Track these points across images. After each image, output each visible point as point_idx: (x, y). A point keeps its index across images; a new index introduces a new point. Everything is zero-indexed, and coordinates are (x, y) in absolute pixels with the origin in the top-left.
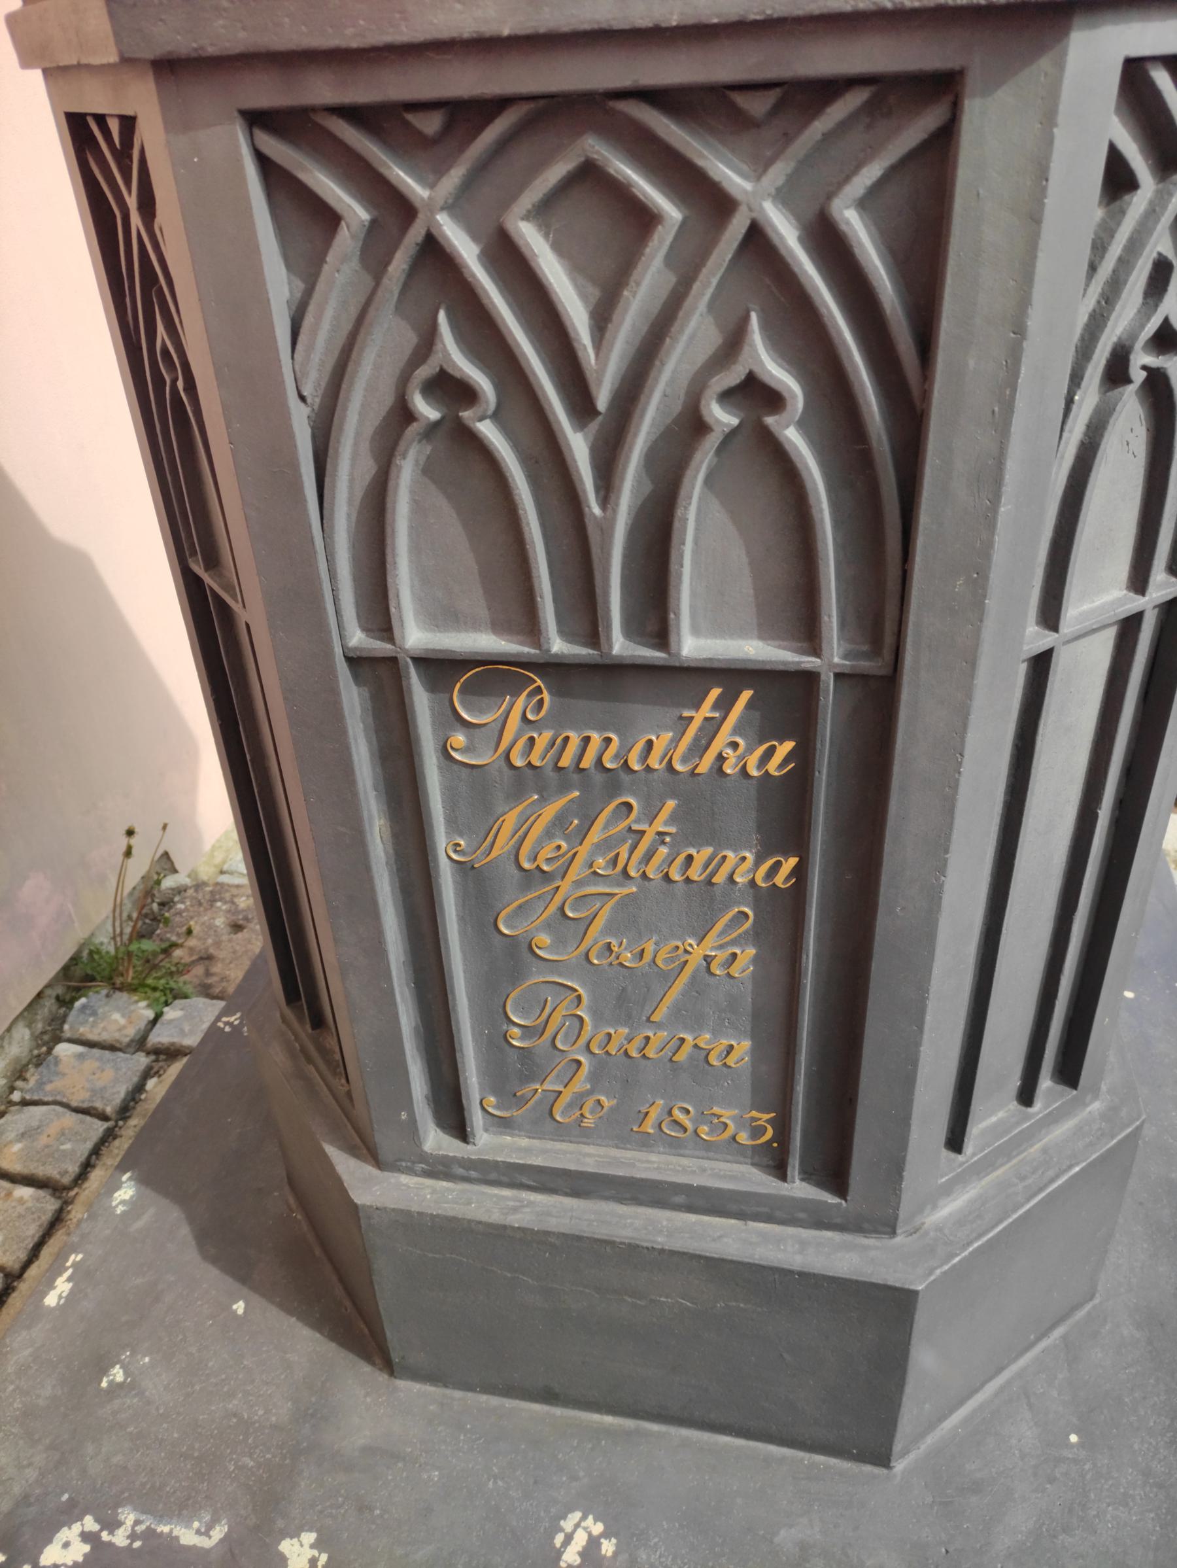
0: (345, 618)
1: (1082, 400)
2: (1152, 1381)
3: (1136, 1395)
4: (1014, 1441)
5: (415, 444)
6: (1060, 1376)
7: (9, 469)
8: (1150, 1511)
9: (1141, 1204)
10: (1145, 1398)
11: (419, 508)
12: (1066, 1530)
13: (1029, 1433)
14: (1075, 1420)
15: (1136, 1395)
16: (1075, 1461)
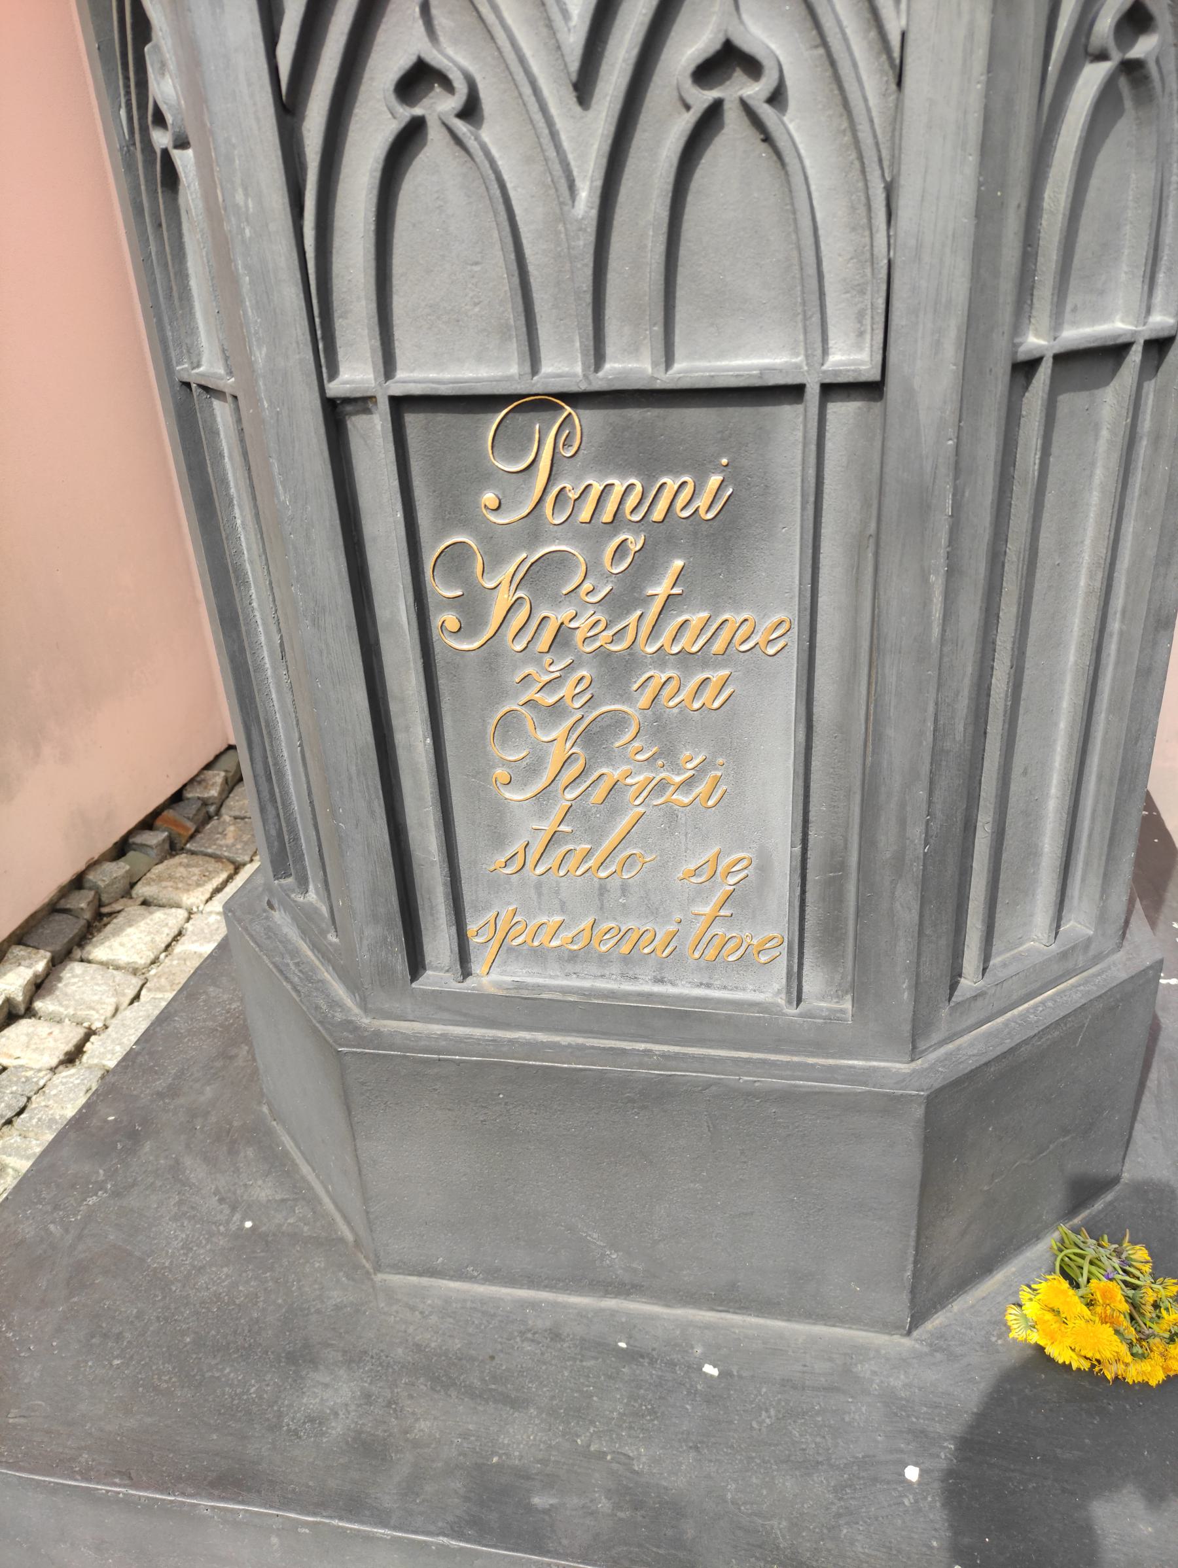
0: (820, 585)
1: (196, 90)
2: (280, 1301)
3: (270, 1284)
4: (260, 1182)
5: (786, 119)
6: (306, 1228)
7: (391, 7)
8: (171, 1263)
9: (492, 1358)
10: (266, 1289)
11: (163, 197)
12: (180, 1203)
13: (263, 1194)
14: (264, 1229)
15: (270, 1284)
16: (228, 1222)
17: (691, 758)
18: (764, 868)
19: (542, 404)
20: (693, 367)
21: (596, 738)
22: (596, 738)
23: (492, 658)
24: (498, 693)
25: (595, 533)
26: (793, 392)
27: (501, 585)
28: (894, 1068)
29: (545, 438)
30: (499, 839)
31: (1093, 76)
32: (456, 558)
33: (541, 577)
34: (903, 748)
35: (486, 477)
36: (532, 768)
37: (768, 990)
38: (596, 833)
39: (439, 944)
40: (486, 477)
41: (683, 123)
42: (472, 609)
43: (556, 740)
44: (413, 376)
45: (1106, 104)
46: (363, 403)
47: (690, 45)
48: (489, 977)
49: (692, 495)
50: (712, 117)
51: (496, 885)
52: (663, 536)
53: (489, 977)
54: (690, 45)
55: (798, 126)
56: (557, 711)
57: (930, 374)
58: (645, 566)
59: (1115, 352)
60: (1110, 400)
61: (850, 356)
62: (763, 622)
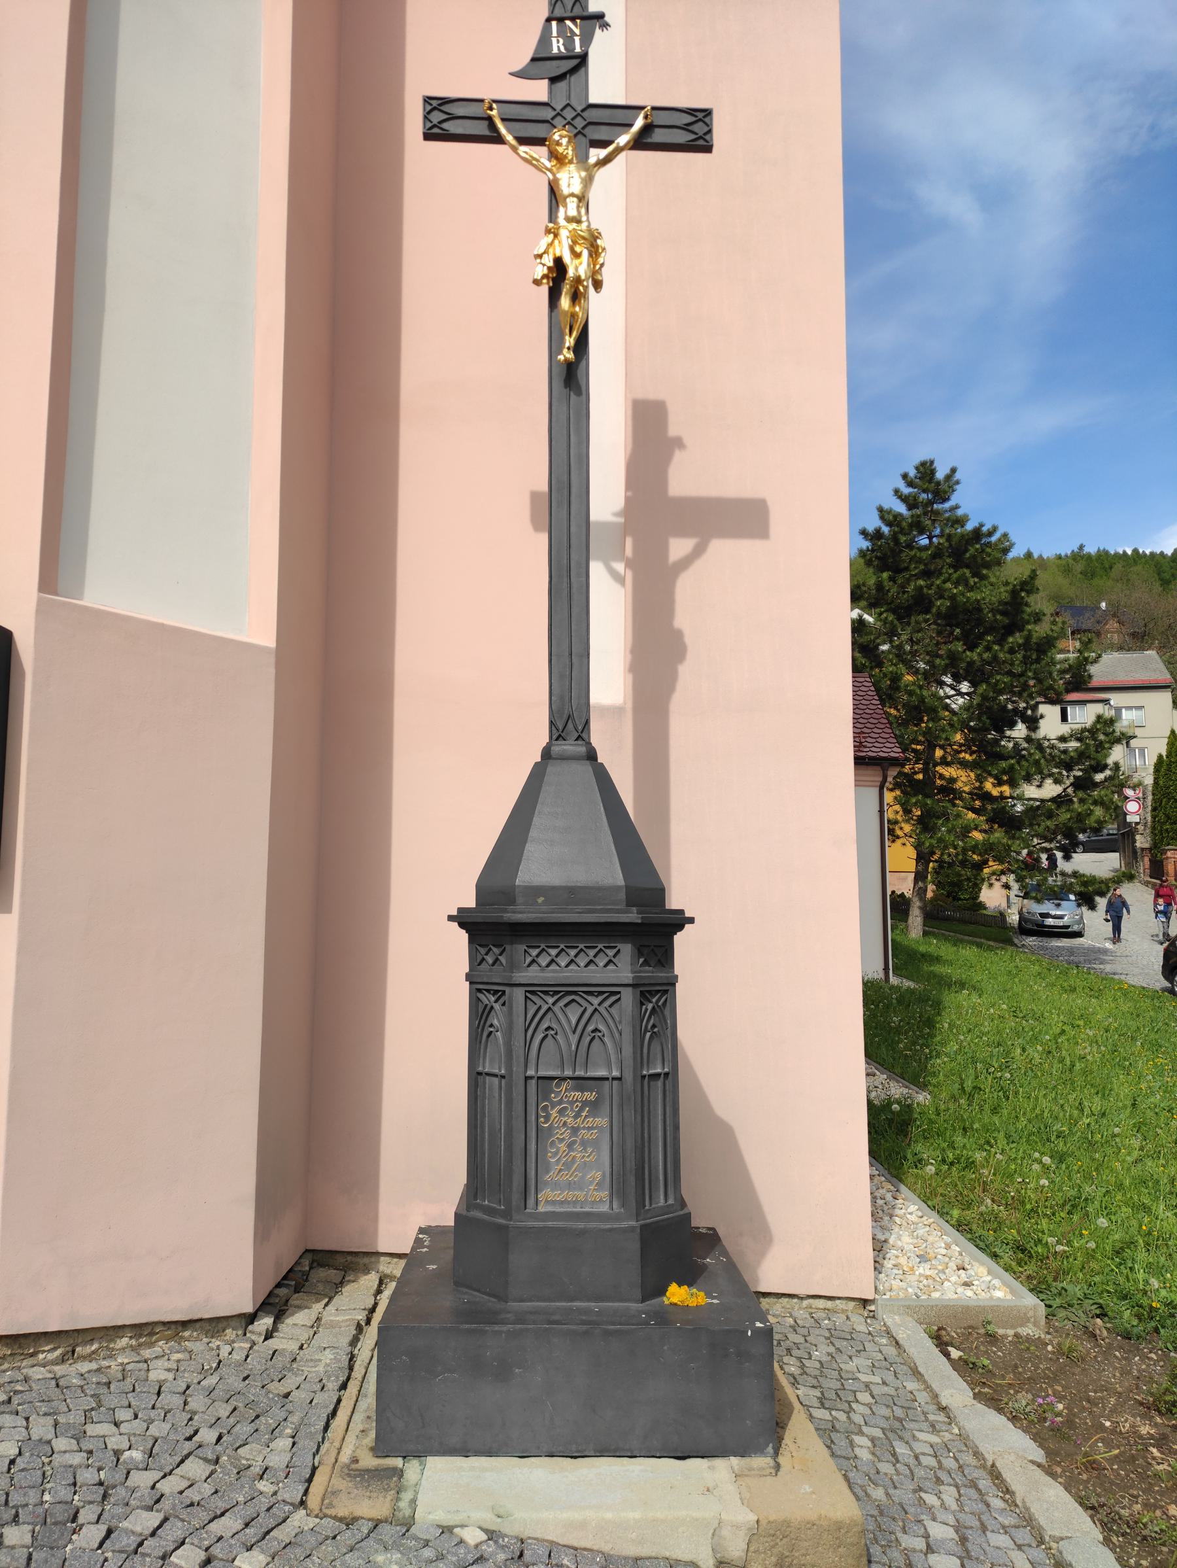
17: (590, 1150)
18: (604, 1175)
19: (564, 1079)
20: (590, 1074)
21: (570, 1146)
22: (570, 1146)
23: (551, 1128)
24: (551, 1135)
25: (572, 1103)
26: (607, 1079)
27: (554, 1113)
28: (633, 1223)
29: (564, 1086)
30: (548, 1172)
31: (648, 1034)
32: (545, 1108)
33: (562, 1112)
34: (630, 1144)
35: (553, 1092)
36: (556, 1154)
37: (604, 1208)
38: (569, 1169)
39: (531, 1202)
40: (553, 1092)
41: (589, 1038)
42: (547, 1118)
43: (562, 1146)
44: (541, 1073)
45: (651, 1037)
46: (531, 1078)
47: (591, 1028)
48: (541, 1209)
49: (590, 1096)
50: (546, 1036)
51: (546, 1183)
52: (585, 1103)
53: (541, 1209)
54: (591, 1028)
55: (606, 1039)
56: (563, 1139)
57: (629, 1077)
58: (581, 1109)
59: (658, 1075)
60: (660, 1083)
61: (616, 1073)
62: (602, 1121)
